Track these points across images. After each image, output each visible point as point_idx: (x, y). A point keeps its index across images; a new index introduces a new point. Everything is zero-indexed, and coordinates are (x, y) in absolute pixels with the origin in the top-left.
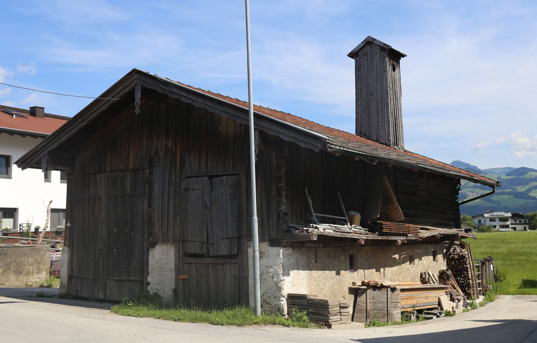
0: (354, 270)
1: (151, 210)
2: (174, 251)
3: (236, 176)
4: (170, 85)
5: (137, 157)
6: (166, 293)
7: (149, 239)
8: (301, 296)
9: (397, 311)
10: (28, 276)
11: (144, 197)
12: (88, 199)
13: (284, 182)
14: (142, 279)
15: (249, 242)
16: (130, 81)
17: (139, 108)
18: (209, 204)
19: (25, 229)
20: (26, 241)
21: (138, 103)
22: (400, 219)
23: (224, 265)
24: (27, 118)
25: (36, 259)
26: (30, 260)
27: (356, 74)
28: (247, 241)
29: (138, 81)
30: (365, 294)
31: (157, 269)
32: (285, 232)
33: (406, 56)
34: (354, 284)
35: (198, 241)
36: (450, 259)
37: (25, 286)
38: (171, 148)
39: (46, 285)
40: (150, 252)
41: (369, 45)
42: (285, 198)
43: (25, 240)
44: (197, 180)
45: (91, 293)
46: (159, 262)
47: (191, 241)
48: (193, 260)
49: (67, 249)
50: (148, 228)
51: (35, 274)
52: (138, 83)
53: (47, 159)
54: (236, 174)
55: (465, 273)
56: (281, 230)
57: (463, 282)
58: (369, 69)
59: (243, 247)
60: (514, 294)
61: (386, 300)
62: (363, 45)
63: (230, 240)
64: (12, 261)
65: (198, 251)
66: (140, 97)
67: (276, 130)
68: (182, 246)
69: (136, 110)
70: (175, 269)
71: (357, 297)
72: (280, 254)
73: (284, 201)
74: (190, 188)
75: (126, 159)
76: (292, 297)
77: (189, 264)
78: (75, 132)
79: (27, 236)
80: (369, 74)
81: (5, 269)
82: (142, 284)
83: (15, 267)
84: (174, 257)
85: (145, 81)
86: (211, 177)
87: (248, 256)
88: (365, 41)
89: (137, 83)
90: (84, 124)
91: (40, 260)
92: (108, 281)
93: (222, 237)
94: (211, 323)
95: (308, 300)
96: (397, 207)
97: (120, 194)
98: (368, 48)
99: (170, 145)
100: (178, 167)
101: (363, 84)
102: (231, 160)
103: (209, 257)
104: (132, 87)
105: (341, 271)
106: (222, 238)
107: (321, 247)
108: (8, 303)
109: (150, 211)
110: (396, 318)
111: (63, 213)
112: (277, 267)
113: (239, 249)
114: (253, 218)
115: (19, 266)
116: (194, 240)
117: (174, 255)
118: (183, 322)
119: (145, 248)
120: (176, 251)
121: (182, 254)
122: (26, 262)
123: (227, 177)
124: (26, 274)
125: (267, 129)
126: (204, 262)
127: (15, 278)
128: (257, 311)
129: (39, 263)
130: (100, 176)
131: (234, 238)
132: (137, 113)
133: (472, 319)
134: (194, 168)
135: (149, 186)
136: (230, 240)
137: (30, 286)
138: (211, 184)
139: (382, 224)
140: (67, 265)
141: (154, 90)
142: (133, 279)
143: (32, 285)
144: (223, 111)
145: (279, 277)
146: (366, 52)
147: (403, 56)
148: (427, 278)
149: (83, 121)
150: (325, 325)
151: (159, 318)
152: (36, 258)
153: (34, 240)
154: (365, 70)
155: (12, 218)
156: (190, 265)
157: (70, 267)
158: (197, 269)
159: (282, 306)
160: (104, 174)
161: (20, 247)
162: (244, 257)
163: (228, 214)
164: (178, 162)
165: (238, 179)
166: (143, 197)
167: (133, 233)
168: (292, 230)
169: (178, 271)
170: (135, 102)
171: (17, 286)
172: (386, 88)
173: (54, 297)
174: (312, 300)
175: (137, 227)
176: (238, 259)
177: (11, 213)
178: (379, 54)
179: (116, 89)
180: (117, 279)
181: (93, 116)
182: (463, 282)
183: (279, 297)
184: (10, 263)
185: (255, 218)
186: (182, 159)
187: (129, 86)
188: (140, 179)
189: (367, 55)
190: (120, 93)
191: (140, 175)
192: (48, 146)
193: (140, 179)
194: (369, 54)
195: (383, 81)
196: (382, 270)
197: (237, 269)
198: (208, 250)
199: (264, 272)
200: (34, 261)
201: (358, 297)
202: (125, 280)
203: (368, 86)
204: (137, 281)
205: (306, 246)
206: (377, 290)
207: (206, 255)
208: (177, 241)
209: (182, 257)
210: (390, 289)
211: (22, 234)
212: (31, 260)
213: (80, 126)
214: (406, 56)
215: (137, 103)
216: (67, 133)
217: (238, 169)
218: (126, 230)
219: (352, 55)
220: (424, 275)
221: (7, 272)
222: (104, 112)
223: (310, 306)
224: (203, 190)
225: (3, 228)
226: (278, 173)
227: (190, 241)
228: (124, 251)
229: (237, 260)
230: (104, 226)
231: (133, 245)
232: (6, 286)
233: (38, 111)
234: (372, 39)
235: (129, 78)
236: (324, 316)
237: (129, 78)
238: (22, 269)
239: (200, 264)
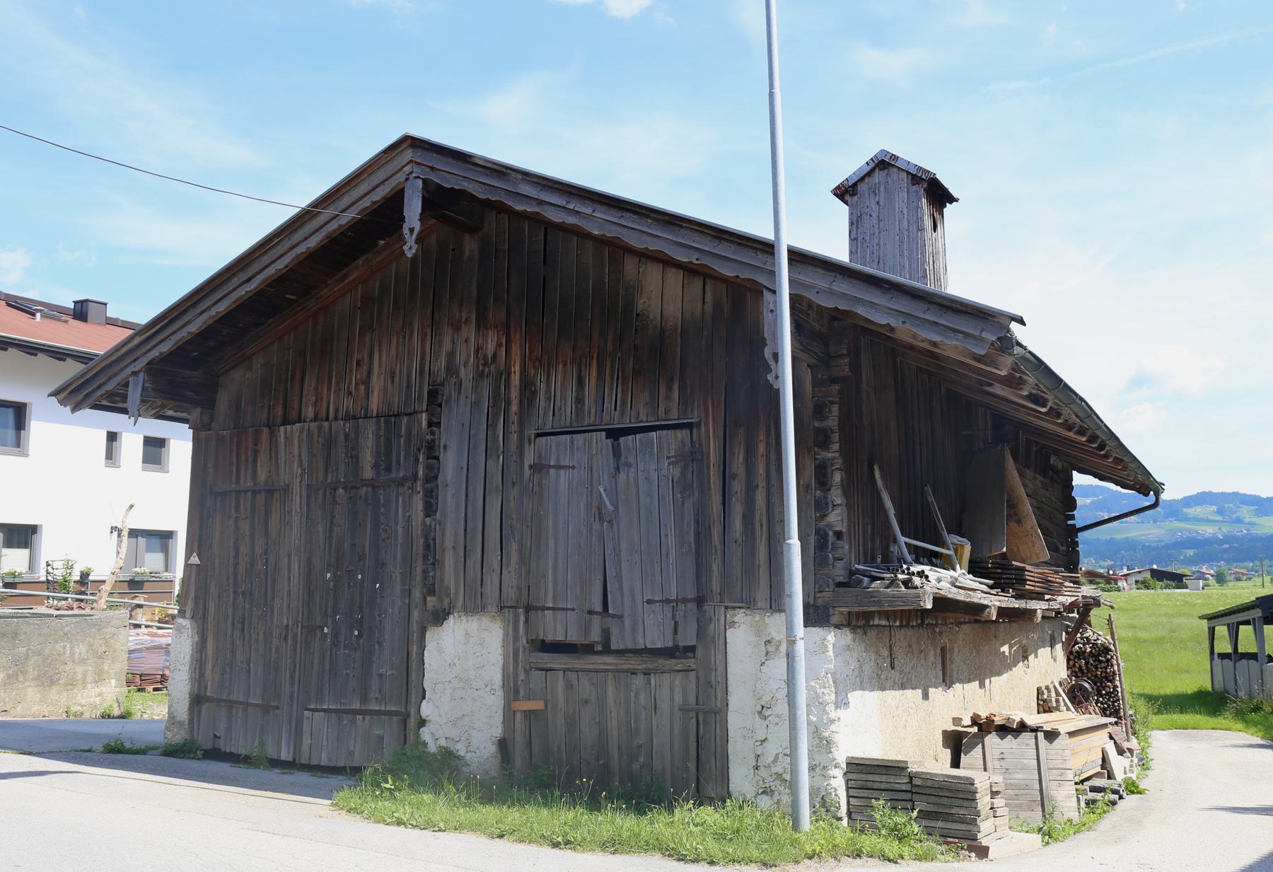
0: (946, 685)
1: (433, 524)
2: (501, 636)
3: (688, 432)
4: (513, 175)
5: (393, 382)
6: (478, 748)
7: (425, 599)
8: (889, 764)
9: (1067, 792)
10: (72, 690)
11: (412, 489)
12: (249, 493)
13: (836, 447)
14: (403, 710)
15: (730, 612)
16: (391, 168)
17: (416, 243)
18: (610, 508)
19: (59, 574)
20: (63, 602)
21: (414, 228)
22: (1038, 558)
23: (652, 675)
24: (66, 322)
25: (94, 647)
26: (78, 651)
27: (852, 235)
28: (723, 609)
29: (415, 170)
30: (980, 746)
31: (450, 682)
32: (839, 585)
33: (956, 200)
34: (957, 721)
35: (573, 609)
36: (1074, 654)
37: (64, 715)
38: (495, 356)
39: (116, 712)
40: (428, 635)
41: (883, 169)
42: (839, 492)
43: (60, 599)
44: (572, 441)
45: (256, 744)
46: (454, 664)
47: (553, 609)
48: (557, 661)
49: (188, 626)
50: (425, 572)
51: (89, 686)
52: (414, 175)
53: (144, 382)
54: (689, 426)
55: (1109, 687)
56: (830, 580)
57: (1106, 706)
58: (882, 223)
59: (712, 626)
60: (1164, 728)
61: (1035, 762)
62: (868, 169)
63: (673, 607)
64: (32, 652)
65: (574, 637)
66: (419, 210)
67: (844, 294)
68: (527, 621)
69: (405, 248)
70: (504, 684)
71: (960, 755)
72: (826, 646)
73: (838, 501)
74: (552, 464)
75: (362, 387)
76: (860, 767)
77: (544, 672)
78: (225, 310)
79: (64, 589)
80: (882, 233)
81: (13, 672)
82: (404, 723)
83: (39, 666)
84: (500, 651)
85: (436, 167)
86: (614, 434)
87: (726, 653)
88: (874, 161)
89: (411, 173)
90: (252, 287)
91: (104, 649)
92: (306, 712)
93: (649, 597)
94: (673, 856)
95: (911, 777)
96: (1032, 528)
97: (342, 480)
98: (879, 176)
99: (490, 347)
100: (514, 408)
101: (868, 256)
102: (676, 387)
103: (607, 650)
104: (396, 186)
105: (930, 689)
106: (649, 602)
107: (897, 627)
108: (26, 778)
109: (430, 525)
110: (1066, 809)
111: (145, 539)
112: (819, 684)
113: (701, 632)
114: (789, 544)
115: (49, 665)
116: (560, 606)
117: (500, 645)
118: (583, 852)
119: (415, 627)
120: (506, 635)
121: (525, 642)
122: (67, 656)
123: (664, 432)
124: (66, 685)
125: (818, 293)
126: (590, 667)
127: (39, 695)
128: (801, 816)
129: (100, 657)
130: (286, 434)
131: (685, 601)
132: (409, 255)
133: (1216, 804)
134: (563, 409)
135: (428, 458)
136: (673, 607)
137: (75, 715)
138: (617, 453)
139: (1023, 569)
140: (187, 668)
141: (462, 193)
142: (377, 708)
143: (82, 714)
144: (675, 242)
145: (824, 710)
146: (875, 184)
147: (952, 199)
148: (1053, 700)
149: (249, 280)
150: (970, 849)
151: (501, 836)
152: (92, 645)
153: (81, 600)
154: (872, 226)
155: (26, 547)
156: (549, 672)
157: (197, 671)
158: (569, 687)
159: (833, 794)
160: (297, 424)
161: (51, 616)
162: (713, 654)
163: (666, 535)
164: (514, 394)
165: (694, 439)
166: (408, 490)
167: (378, 585)
168: (861, 581)
169: (512, 690)
170: (404, 226)
171: (44, 716)
172: (923, 265)
173: (151, 752)
174: (924, 776)
175: (392, 569)
176: (691, 660)
177: (21, 536)
178: (906, 190)
179: (349, 190)
180: (330, 707)
181: (281, 265)
182: (1106, 706)
183: (824, 767)
184: (27, 657)
185: (794, 543)
186: (528, 389)
187: (386, 183)
188: (402, 440)
189: (877, 191)
190: (361, 202)
191: (403, 427)
192: (144, 350)
193: (402, 440)
194: (882, 189)
195: (915, 251)
196: (987, 681)
197: (693, 685)
198: (606, 634)
199: (777, 695)
200: (87, 652)
201: (962, 754)
202: (355, 712)
203: (879, 262)
204: (389, 714)
205: (874, 625)
206: (1009, 736)
207: (600, 648)
208: (511, 607)
209: (524, 651)
210: (1042, 733)
211: (49, 584)
212: (81, 649)
213: (241, 292)
214: (956, 200)
215: (410, 229)
216: (201, 313)
217: (696, 412)
218: (360, 577)
219: (844, 192)
220: (1045, 691)
221: (18, 681)
222: (312, 256)
223: (916, 793)
224: (592, 468)
225: (6, 570)
226: (816, 424)
227: (549, 609)
228: (352, 632)
229: (691, 663)
230: (296, 564)
231: (379, 615)
232: (14, 717)
233: (92, 310)
234: (891, 157)
235: (389, 161)
236: (962, 821)
237: (389, 161)
238: (57, 674)
239: (577, 672)
